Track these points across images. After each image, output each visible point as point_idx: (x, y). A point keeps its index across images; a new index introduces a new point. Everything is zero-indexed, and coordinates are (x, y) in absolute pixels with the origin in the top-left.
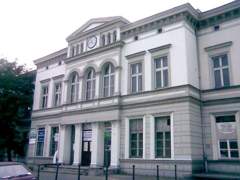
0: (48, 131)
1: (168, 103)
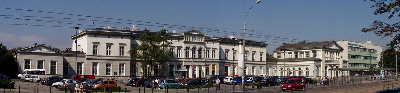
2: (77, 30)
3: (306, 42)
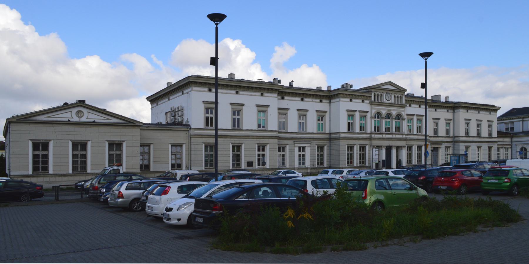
2: (426, 59)
3: (86, 103)
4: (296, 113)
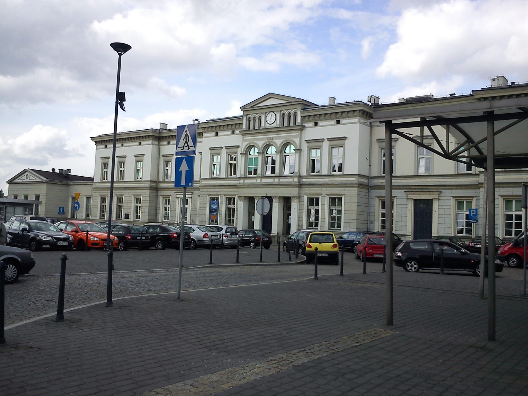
0: (223, 202)
1: (341, 187)
4: (134, 159)
